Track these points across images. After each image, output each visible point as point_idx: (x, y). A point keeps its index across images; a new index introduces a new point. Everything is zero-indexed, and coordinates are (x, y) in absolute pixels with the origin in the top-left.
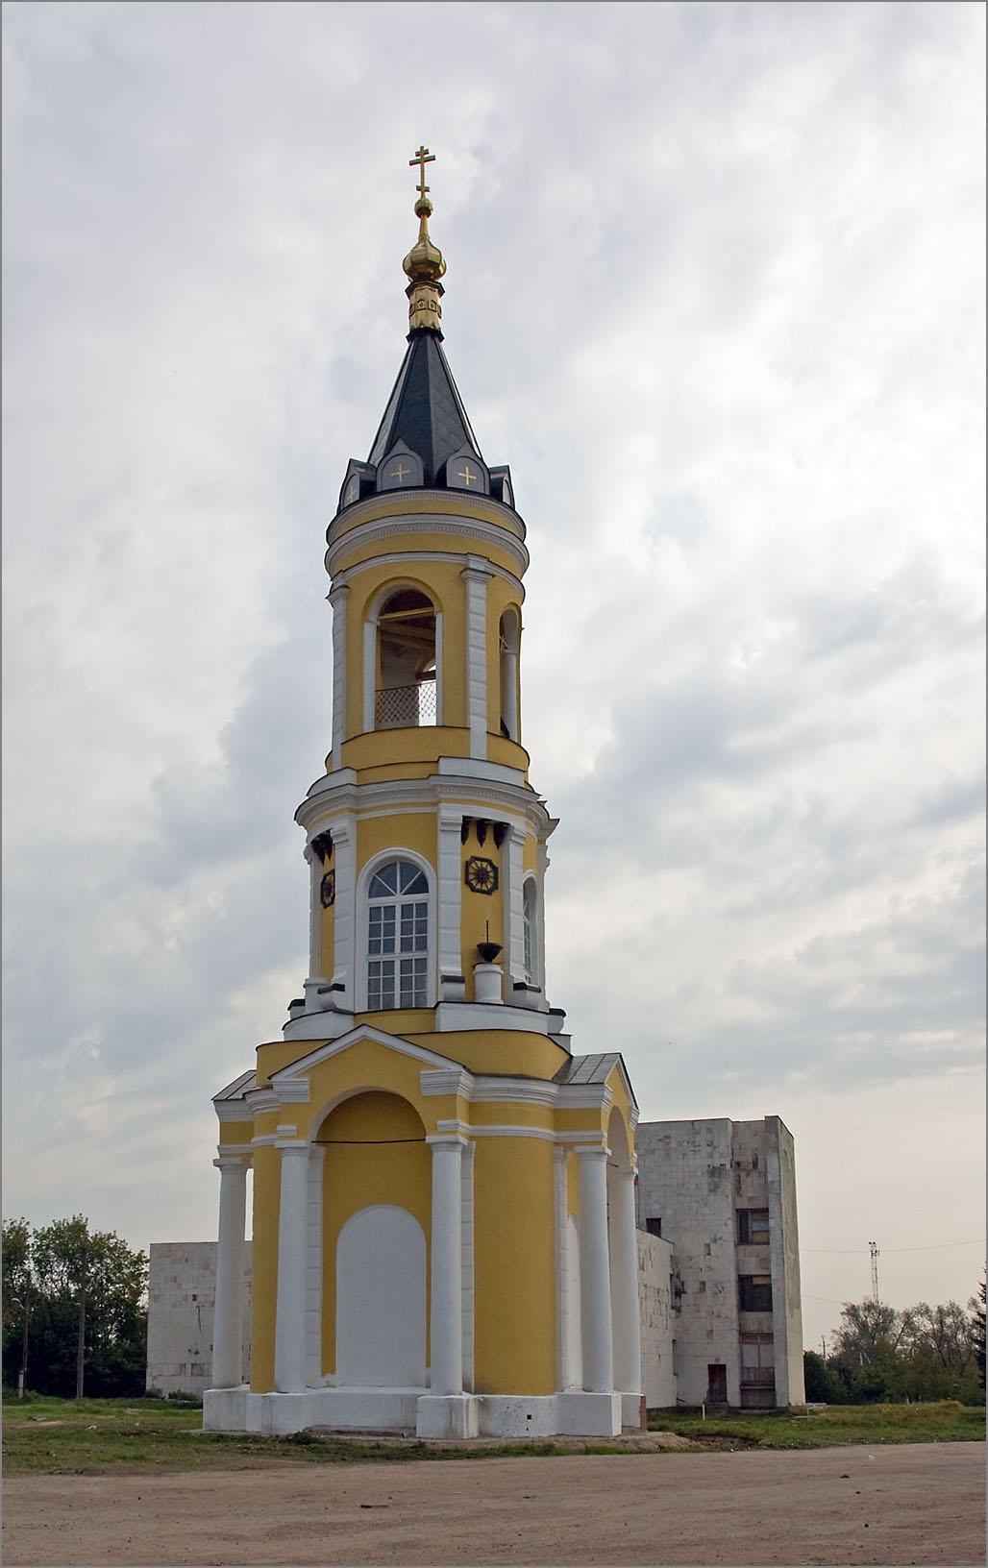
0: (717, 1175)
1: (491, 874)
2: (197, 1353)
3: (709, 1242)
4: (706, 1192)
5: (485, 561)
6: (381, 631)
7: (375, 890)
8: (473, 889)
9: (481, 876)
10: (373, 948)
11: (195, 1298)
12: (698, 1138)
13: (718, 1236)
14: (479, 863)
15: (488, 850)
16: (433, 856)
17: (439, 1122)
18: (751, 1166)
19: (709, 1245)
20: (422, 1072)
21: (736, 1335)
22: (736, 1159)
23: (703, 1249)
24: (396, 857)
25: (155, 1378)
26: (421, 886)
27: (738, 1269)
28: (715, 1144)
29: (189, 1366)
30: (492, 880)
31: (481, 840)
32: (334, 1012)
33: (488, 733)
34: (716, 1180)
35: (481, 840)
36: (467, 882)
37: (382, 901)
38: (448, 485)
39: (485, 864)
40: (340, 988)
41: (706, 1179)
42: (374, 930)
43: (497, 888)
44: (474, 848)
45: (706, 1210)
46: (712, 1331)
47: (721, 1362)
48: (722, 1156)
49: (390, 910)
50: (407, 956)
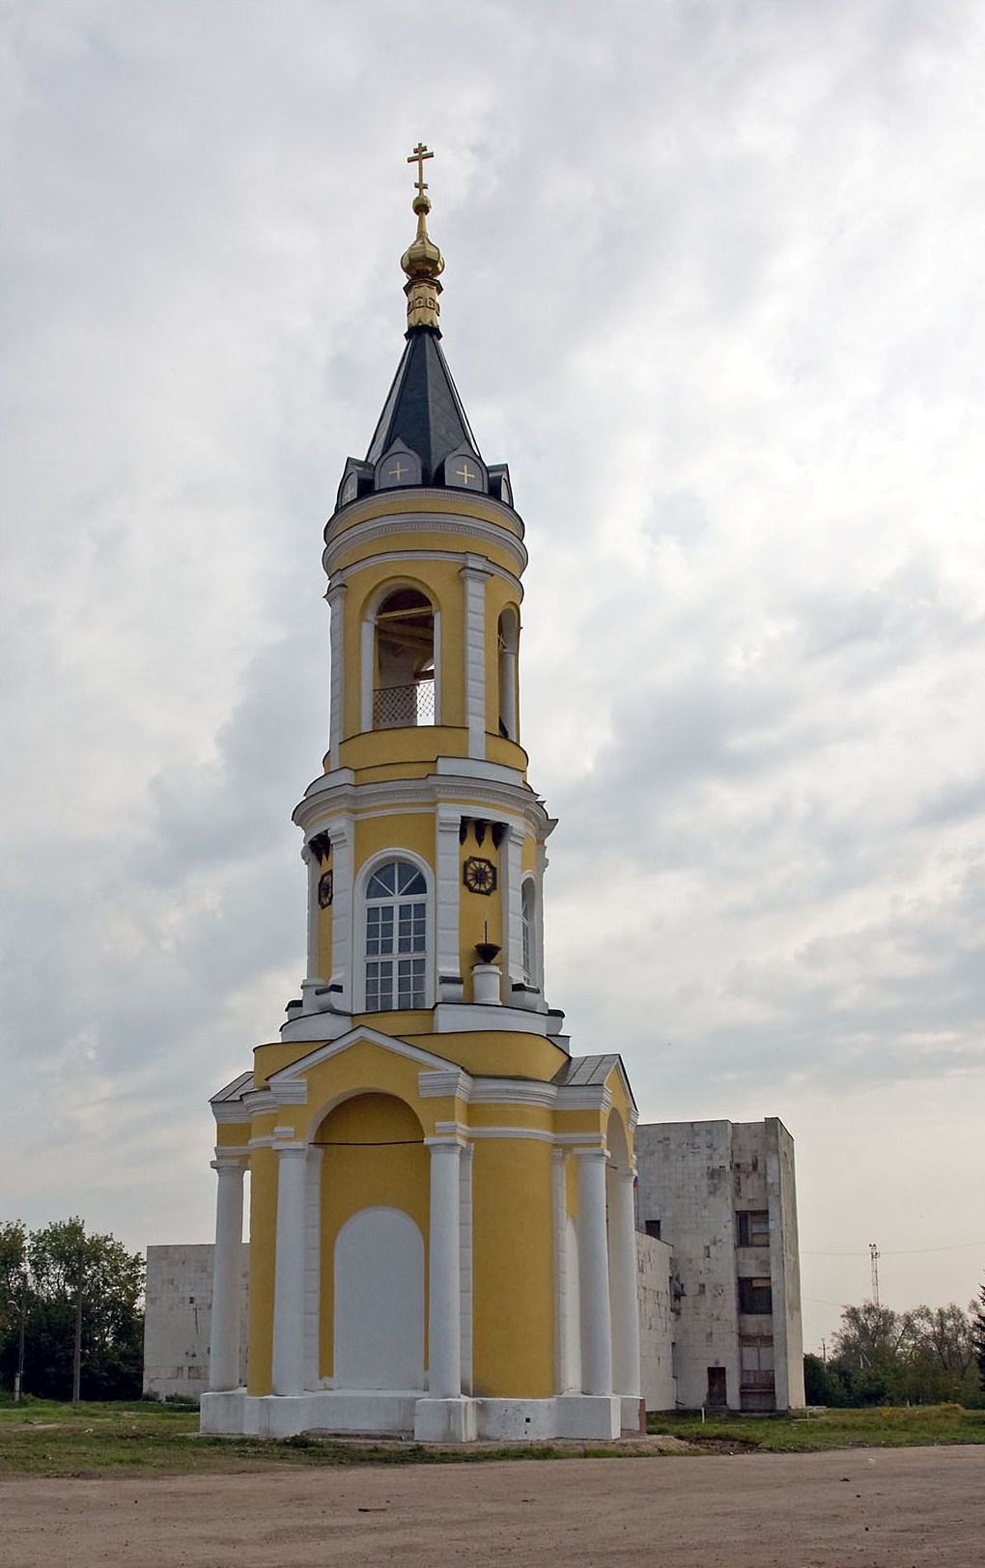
0: (716, 1176)
1: (490, 875)
2: (194, 1356)
3: (708, 1244)
4: (705, 1195)
5: (484, 560)
6: (379, 630)
7: (373, 890)
8: (472, 890)
9: (480, 876)
10: (371, 949)
11: (192, 1300)
12: (698, 1140)
13: (718, 1238)
14: (483, 889)
15: (486, 850)
16: (432, 859)
17: (437, 1124)
18: (751, 1168)
19: (708, 1248)
20: (420, 1074)
21: (735, 1337)
22: (736, 1161)
23: (702, 1252)
24: (394, 857)
25: (152, 1380)
26: (419, 886)
27: (737, 1271)
28: (715, 1146)
29: (186, 1369)
30: (490, 881)
31: (480, 841)
32: (332, 1013)
33: (486, 732)
34: (716, 1181)
35: (480, 841)
36: (466, 883)
37: (380, 958)
38: (447, 484)
39: (483, 865)
40: (338, 989)
41: (705, 1181)
42: (371, 931)
43: (495, 889)
44: (472, 848)
45: (706, 1213)
46: (711, 1333)
47: (721, 1366)
48: (721, 1158)
49: (388, 910)
50: (405, 957)
